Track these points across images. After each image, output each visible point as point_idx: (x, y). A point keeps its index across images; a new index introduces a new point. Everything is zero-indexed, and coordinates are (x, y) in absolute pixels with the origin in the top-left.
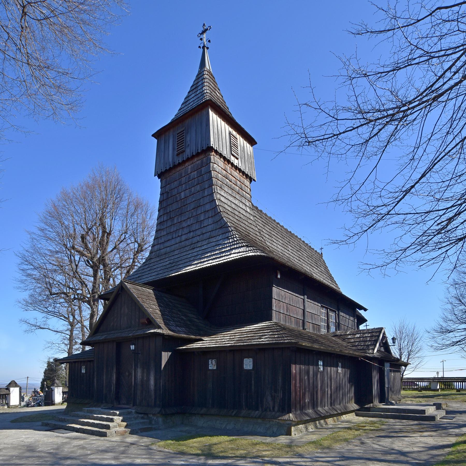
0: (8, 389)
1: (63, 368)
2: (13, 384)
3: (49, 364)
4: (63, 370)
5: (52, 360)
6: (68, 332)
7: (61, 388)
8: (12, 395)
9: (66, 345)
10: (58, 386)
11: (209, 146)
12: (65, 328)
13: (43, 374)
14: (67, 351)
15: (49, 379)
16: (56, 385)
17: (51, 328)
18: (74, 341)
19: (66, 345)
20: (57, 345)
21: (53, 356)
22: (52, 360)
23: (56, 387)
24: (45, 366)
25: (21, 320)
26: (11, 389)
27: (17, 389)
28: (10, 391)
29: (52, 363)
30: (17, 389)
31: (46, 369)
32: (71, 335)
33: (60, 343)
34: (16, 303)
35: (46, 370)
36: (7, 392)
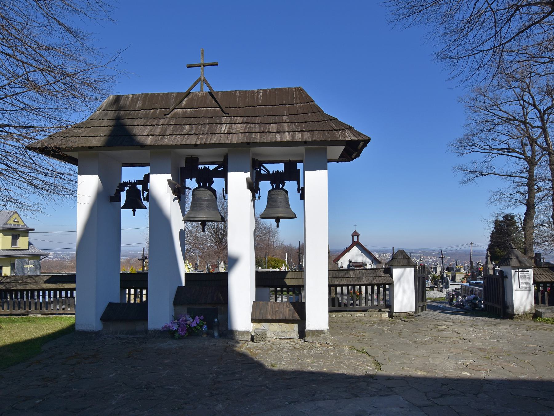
0: (388, 271)
1: (520, 229)
2: (401, 258)
3: (497, 223)
4: (520, 232)
5: (501, 218)
6: (525, 175)
7: (531, 271)
8: (397, 289)
9: (522, 194)
10: (522, 266)
11: (488, 274)
12: (520, 168)
13: (489, 239)
14: (525, 202)
15: (498, 246)
16: (514, 262)
17: (497, 171)
18: (536, 187)
19: (522, 194)
20: (509, 196)
21: (503, 211)
22: (501, 218)
23: (514, 268)
24: (492, 227)
25: (455, 168)
26: (396, 272)
27: (410, 273)
28: (392, 276)
29: (502, 222)
30: (410, 273)
31: (493, 231)
32: (531, 178)
33: (511, 192)
34: (449, 147)
35: (493, 233)
36: (383, 277)
